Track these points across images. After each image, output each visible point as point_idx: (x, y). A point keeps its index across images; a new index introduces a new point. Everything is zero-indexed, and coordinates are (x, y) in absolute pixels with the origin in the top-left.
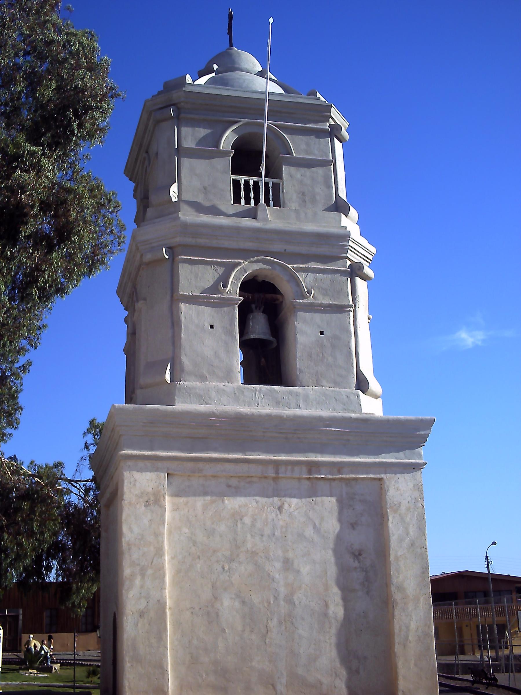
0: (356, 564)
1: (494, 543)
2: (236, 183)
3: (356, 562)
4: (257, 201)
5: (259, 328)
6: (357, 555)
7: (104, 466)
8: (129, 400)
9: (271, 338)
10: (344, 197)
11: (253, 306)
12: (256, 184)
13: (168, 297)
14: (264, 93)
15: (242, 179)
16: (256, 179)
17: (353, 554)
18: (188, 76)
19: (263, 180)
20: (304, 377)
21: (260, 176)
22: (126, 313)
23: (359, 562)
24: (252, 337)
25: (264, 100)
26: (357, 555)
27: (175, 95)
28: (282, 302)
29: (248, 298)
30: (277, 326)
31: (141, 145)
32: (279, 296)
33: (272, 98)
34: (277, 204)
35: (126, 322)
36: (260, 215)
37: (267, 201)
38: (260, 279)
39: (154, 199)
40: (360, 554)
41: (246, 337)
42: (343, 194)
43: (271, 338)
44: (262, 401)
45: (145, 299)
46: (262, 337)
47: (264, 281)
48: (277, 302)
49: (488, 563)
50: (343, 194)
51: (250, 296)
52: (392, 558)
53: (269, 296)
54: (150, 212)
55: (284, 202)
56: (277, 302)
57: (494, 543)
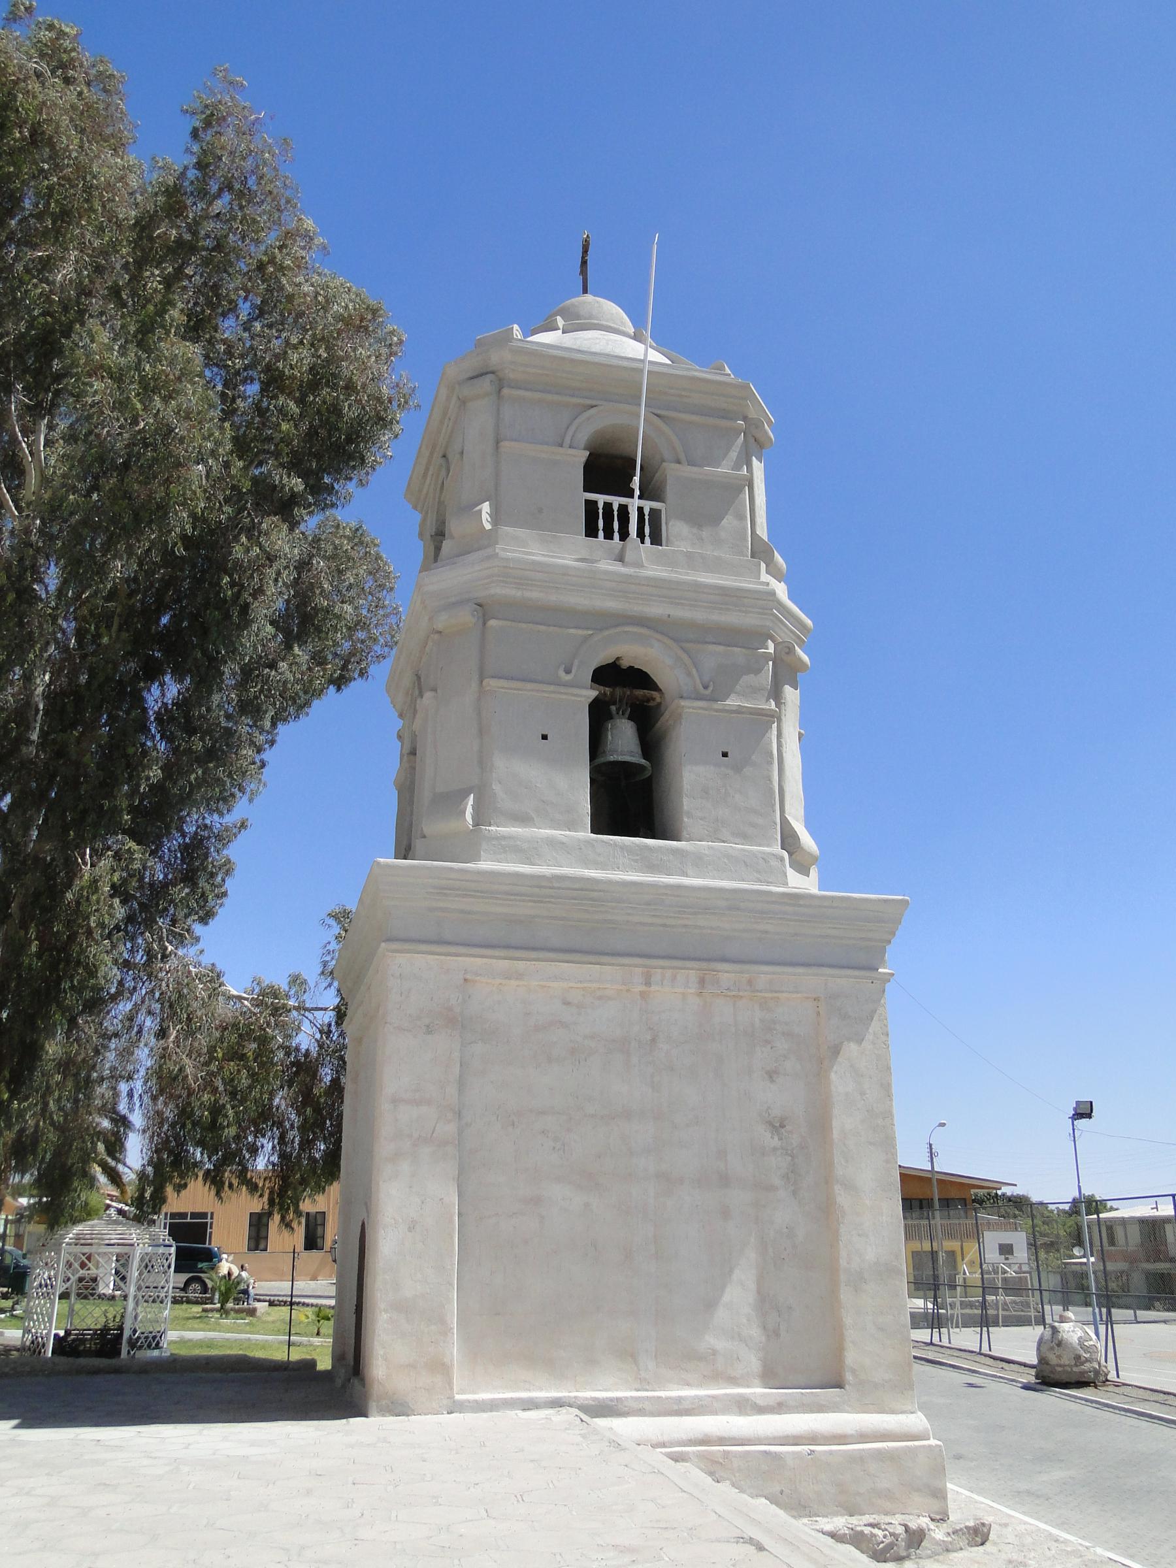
0: (776, 1142)
1: (943, 1125)
2: (591, 506)
3: (776, 1138)
4: (624, 535)
5: (624, 741)
6: (778, 1126)
7: (351, 974)
8: (405, 850)
9: (643, 762)
10: (765, 538)
11: (613, 708)
12: (624, 509)
13: (474, 685)
14: (642, 361)
15: (601, 499)
16: (624, 500)
17: (770, 1124)
18: (516, 327)
19: (634, 504)
20: (688, 823)
21: (632, 496)
22: (400, 723)
23: (780, 1139)
24: (612, 758)
25: (642, 371)
26: (778, 1126)
27: (495, 358)
28: (659, 704)
29: (605, 694)
30: (651, 742)
31: (434, 447)
32: (655, 694)
33: (656, 369)
34: (656, 540)
35: (400, 737)
36: (629, 556)
37: (641, 534)
38: (625, 664)
39: (455, 527)
40: (782, 1126)
41: (601, 760)
42: (763, 532)
43: (643, 762)
44: (623, 862)
45: (434, 690)
46: (628, 758)
47: (631, 668)
48: (651, 704)
49: (932, 1156)
50: (763, 532)
51: (608, 690)
52: (836, 1134)
53: (640, 693)
54: (447, 546)
55: (194, 1215)
56: (651, 704)
57: (1083, 1112)
